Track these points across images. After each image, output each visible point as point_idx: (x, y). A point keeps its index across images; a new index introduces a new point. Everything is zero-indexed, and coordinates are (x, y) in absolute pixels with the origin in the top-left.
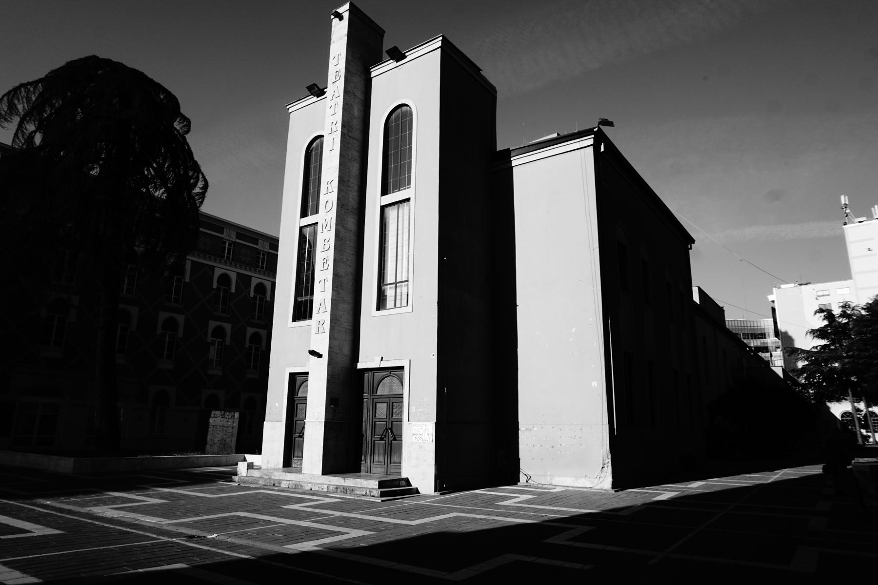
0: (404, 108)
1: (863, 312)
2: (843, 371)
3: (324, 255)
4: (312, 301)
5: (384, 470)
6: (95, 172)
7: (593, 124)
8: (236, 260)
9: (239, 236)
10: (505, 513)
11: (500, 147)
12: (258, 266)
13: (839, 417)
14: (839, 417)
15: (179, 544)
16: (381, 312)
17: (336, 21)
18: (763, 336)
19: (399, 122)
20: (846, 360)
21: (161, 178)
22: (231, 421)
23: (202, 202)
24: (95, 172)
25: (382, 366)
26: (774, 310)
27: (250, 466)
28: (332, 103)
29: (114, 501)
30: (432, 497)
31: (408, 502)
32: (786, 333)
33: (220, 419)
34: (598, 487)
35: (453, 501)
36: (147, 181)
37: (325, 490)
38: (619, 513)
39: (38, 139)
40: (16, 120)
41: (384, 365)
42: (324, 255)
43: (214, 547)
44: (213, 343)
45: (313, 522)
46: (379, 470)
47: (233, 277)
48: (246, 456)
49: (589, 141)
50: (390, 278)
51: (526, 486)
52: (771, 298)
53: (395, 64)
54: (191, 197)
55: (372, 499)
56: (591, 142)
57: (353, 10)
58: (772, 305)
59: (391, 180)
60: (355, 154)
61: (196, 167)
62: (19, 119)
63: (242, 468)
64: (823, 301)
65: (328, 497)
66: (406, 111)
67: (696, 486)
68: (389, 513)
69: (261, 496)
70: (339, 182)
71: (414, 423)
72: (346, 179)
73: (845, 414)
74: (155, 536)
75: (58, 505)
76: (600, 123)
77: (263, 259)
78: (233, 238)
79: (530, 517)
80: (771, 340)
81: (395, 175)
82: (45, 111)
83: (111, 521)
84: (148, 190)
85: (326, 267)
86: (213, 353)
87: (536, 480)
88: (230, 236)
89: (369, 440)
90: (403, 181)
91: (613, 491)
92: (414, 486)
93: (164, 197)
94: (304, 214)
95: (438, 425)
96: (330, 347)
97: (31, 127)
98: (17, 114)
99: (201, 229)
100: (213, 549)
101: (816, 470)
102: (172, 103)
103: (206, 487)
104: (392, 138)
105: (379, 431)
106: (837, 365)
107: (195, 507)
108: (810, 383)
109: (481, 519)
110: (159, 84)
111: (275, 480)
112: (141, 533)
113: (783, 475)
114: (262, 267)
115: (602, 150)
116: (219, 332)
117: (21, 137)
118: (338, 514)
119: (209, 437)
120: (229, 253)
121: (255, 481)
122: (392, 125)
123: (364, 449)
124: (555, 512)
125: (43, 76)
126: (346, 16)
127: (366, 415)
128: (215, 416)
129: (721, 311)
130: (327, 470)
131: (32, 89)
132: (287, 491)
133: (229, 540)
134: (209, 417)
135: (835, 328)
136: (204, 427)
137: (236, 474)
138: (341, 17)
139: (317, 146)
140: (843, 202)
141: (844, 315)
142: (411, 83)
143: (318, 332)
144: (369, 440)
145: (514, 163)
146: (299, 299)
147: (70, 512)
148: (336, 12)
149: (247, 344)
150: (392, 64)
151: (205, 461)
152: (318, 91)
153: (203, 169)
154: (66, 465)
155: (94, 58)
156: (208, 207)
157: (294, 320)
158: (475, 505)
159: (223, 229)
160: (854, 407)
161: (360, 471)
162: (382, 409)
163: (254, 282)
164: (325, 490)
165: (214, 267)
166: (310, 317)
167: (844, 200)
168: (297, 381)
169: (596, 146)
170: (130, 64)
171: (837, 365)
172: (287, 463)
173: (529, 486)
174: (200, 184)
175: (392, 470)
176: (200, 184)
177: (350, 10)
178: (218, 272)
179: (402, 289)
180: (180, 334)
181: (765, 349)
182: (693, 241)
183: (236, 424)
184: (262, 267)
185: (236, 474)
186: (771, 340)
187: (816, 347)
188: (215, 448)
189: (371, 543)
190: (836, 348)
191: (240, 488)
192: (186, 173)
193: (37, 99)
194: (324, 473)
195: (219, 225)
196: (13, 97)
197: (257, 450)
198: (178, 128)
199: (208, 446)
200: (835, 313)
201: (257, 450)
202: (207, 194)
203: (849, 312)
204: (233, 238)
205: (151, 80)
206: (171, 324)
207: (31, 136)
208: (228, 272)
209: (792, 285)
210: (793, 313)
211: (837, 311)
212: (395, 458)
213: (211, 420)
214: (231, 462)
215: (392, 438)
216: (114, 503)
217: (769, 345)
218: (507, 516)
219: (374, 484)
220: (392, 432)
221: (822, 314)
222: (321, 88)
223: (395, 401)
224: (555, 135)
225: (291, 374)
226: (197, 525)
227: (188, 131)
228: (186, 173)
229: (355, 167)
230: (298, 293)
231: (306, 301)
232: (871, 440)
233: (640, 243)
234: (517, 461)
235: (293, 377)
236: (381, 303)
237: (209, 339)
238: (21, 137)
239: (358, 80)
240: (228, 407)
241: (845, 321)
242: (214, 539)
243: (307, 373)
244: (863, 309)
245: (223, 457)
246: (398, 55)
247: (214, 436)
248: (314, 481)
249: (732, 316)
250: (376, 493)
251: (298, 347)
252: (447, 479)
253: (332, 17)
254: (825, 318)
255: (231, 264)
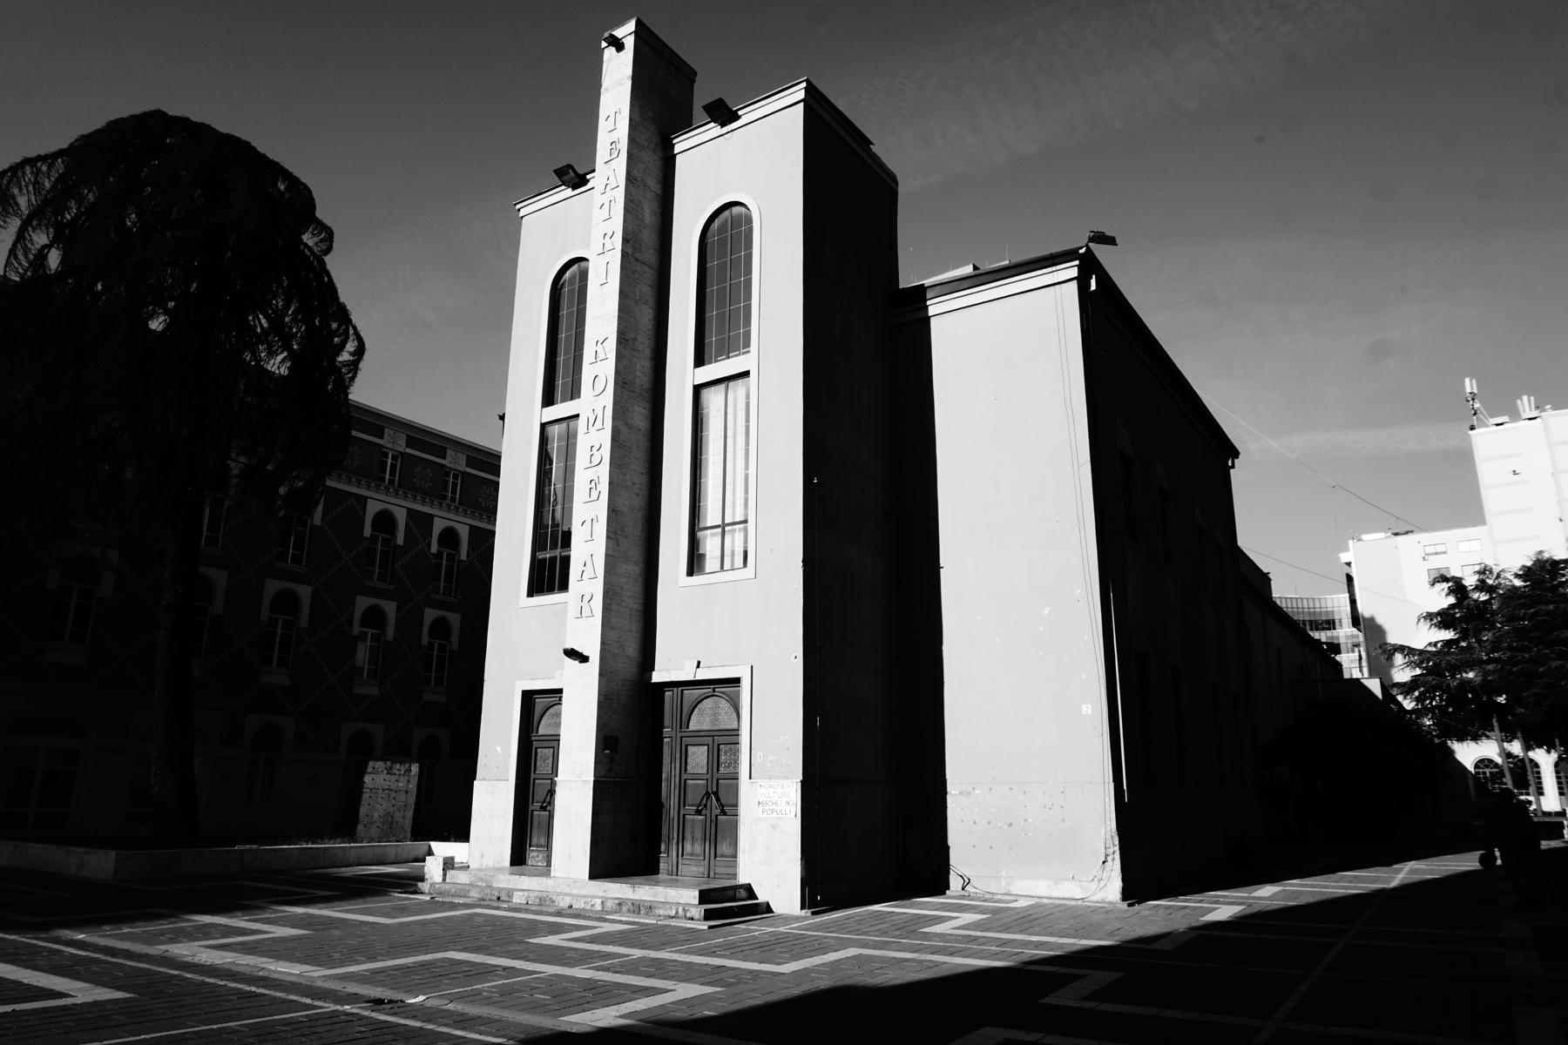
0: (736, 210)
1: (1518, 583)
2: (1487, 688)
3: (591, 474)
4: (566, 561)
5: (702, 869)
6: (156, 325)
7: (1079, 241)
8: (405, 485)
9: (411, 442)
10: (945, 948)
11: (907, 280)
12: (445, 498)
13: (1470, 767)
14: (1471, 768)
15: (361, 1018)
16: (696, 579)
17: (610, 53)
18: (1330, 624)
19: (727, 233)
20: (1490, 667)
21: (279, 332)
22: (404, 780)
23: (352, 379)
24: (156, 325)
25: (699, 677)
26: (1350, 579)
27: (449, 864)
28: (605, 199)
29: (205, 932)
30: (797, 919)
31: (756, 929)
32: (1372, 620)
33: (383, 776)
34: (1095, 898)
35: (839, 926)
36: (253, 340)
37: (599, 908)
38: (1152, 946)
39: (54, 259)
40: (15, 224)
41: (702, 675)
42: (591, 474)
43: (429, 1021)
44: (363, 637)
45: (597, 969)
46: (692, 869)
47: (401, 516)
48: (434, 845)
49: (1070, 271)
50: (711, 516)
51: (962, 897)
52: (1345, 557)
53: (718, 130)
54: (336, 370)
55: (690, 925)
56: (1074, 273)
57: (641, 33)
58: (1347, 569)
59: (712, 339)
60: (646, 290)
61: (343, 315)
62: (19, 222)
63: (433, 868)
64: (1439, 563)
65: (606, 920)
66: (740, 216)
67: (1267, 895)
68: (733, 950)
69: (480, 919)
70: (619, 341)
71: (761, 782)
72: (630, 336)
73: (1483, 763)
74: (308, 1001)
75: (102, 942)
76: (1091, 240)
77: (455, 485)
78: (401, 446)
79: (994, 956)
80: (1345, 632)
81: (721, 327)
82: (68, 209)
83: (212, 970)
84: (256, 357)
85: (594, 496)
86: (362, 655)
87: (979, 886)
88: (394, 443)
89: (674, 813)
90: (736, 341)
91: (1124, 905)
92: (762, 897)
93: (284, 371)
94: (548, 400)
95: (806, 785)
96: (603, 643)
97: (40, 239)
98: (16, 214)
99: (354, 433)
100: (430, 1027)
101: (1469, 862)
102: (300, 202)
103: (371, 903)
104: (712, 264)
105: (694, 797)
106: (1471, 675)
107: (366, 944)
108: (1425, 708)
109: (907, 960)
110: (277, 164)
111: (500, 890)
112: (279, 994)
113: (1411, 872)
114: (453, 500)
115: (1093, 287)
116: (374, 617)
117: (21, 257)
118: (637, 953)
119: (363, 811)
120: (393, 473)
121: (463, 891)
122: (713, 238)
123: (664, 832)
124: (1038, 945)
125: (65, 146)
126: (629, 43)
127: (668, 768)
128: (375, 772)
129: (1265, 579)
130: (601, 868)
131: (44, 168)
132: (527, 911)
133: (451, 1006)
134: (364, 772)
135: (1467, 610)
136: (353, 792)
137: (422, 879)
138: (618, 45)
139: (573, 277)
140: (1468, 390)
141: (1482, 586)
142: (750, 164)
143: (580, 612)
144: (674, 813)
145: (932, 311)
146: (540, 556)
147: (128, 955)
148: (612, 36)
149: (425, 640)
150: (714, 130)
151: (360, 854)
152: (575, 178)
153: (355, 318)
154: (100, 863)
155: (159, 114)
156: (361, 393)
157: (530, 594)
158: (884, 933)
159: (383, 429)
160: (1502, 749)
161: (656, 871)
162: (698, 757)
163: (439, 526)
164: (599, 908)
165: (365, 498)
166: (564, 586)
167: (1470, 385)
168: (537, 706)
169: (1082, 281)
170: (223, 127)
171: (1471, 675)
172: (518, 858)
173: (969, 897)
174: (351, 346)
175: (719, 870)
176: (351, 346)
177: (636, 33)
178: (372, 508)
179: (735, 541)
180: (304, 620)
181: (1335, 648)
182: (1236, 454)
183: (413, 786)
184: (453, 500)
185: (422, 879)
186: (1345, 632)
187: (1435, 645)
188: (374, 831)
189: (723, 1011)
190: (1469, 646)
191: (434, 905)
192: (325, 323)
193: (53, 187)
194: (595, 874)
195: (378, 422)
196: (10, 182)
197: (460, 832)
198: (310, 243)
199: (360, 827)
200: (1466, 583)
201: (460, 832)
202: (361, 365)
203: (1490, 582)
204: (401, 446)
205: (264, 156)
206: (286, 602)
207: (42, 255)
208: (390, 507)
209: (1381, 535)
210: (1377, 580)
211: (1470, 581)
212: (724, 848)
213: (367, 779)
214: (404, 856)
215: (718, 809)
216: (207, 936)
217: (1342, 641)
218: (951, 954)
219: (692, 896)
220: (718, 799)
221: (1445, 586)
222: (581, 172)
223: (724, 742)
224: (967, 270)
225: (524, 692)
226: (379, 977)
227: (329, 250)
228: (326, 329)
229: (646, 316)
230: (538, 542)
231: (553, 559)
232: (1533, 807)
233: (1156, 458)
234: (945, 850)
235: (528, 697)
236: (695, 563)
237: (357, 629)
238: (21, 257)
239: (652, 160)
240: (396, 753)
241: (1484, 597)
242: (421, 1004)
243: (560, 691)
244: (1517, 576)
245: (390, 847)
246: (724, 114)
247: (373, 808)
248: (575, 892)
249: (1283, 591)
250: (697, 912)
251: (538, 645)
252: (825, 883)
253: (604, 44)
254: (1451, 591)
255: (397, 493)
